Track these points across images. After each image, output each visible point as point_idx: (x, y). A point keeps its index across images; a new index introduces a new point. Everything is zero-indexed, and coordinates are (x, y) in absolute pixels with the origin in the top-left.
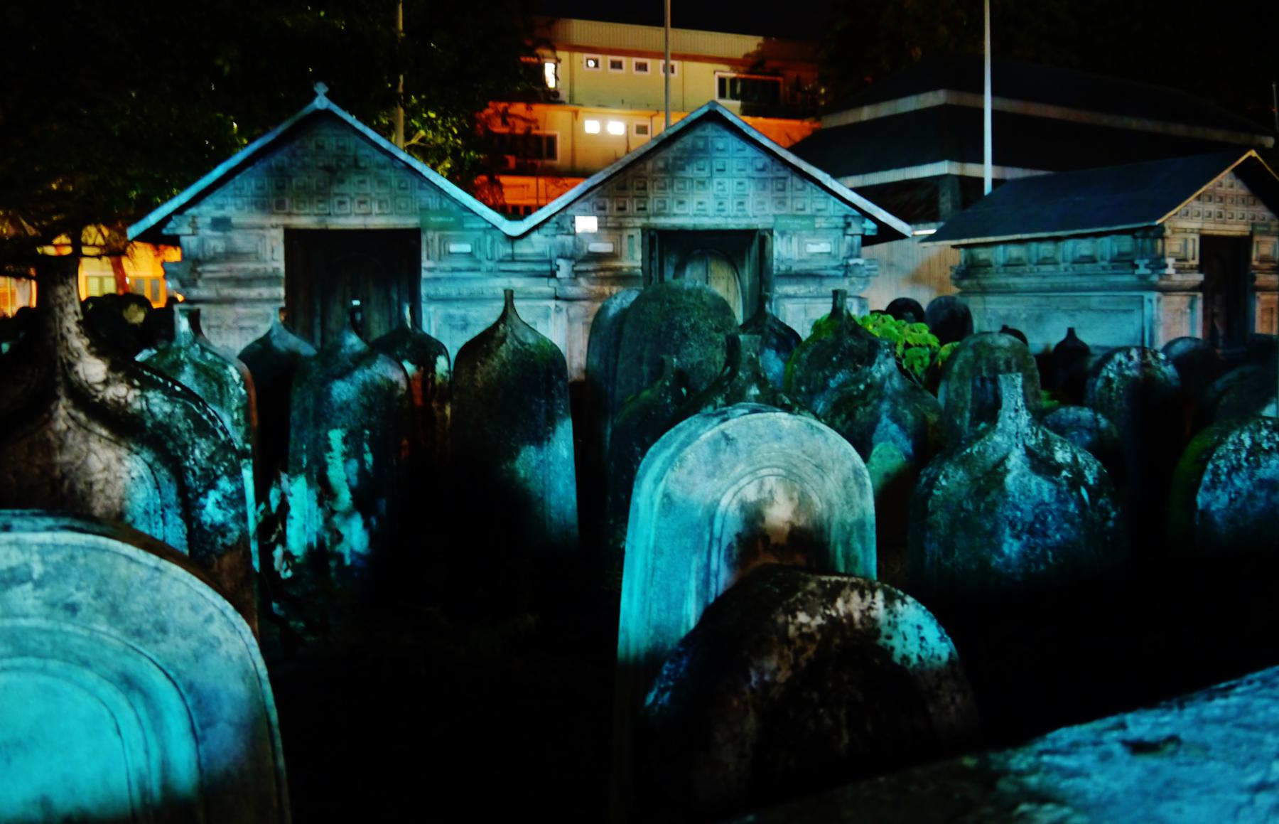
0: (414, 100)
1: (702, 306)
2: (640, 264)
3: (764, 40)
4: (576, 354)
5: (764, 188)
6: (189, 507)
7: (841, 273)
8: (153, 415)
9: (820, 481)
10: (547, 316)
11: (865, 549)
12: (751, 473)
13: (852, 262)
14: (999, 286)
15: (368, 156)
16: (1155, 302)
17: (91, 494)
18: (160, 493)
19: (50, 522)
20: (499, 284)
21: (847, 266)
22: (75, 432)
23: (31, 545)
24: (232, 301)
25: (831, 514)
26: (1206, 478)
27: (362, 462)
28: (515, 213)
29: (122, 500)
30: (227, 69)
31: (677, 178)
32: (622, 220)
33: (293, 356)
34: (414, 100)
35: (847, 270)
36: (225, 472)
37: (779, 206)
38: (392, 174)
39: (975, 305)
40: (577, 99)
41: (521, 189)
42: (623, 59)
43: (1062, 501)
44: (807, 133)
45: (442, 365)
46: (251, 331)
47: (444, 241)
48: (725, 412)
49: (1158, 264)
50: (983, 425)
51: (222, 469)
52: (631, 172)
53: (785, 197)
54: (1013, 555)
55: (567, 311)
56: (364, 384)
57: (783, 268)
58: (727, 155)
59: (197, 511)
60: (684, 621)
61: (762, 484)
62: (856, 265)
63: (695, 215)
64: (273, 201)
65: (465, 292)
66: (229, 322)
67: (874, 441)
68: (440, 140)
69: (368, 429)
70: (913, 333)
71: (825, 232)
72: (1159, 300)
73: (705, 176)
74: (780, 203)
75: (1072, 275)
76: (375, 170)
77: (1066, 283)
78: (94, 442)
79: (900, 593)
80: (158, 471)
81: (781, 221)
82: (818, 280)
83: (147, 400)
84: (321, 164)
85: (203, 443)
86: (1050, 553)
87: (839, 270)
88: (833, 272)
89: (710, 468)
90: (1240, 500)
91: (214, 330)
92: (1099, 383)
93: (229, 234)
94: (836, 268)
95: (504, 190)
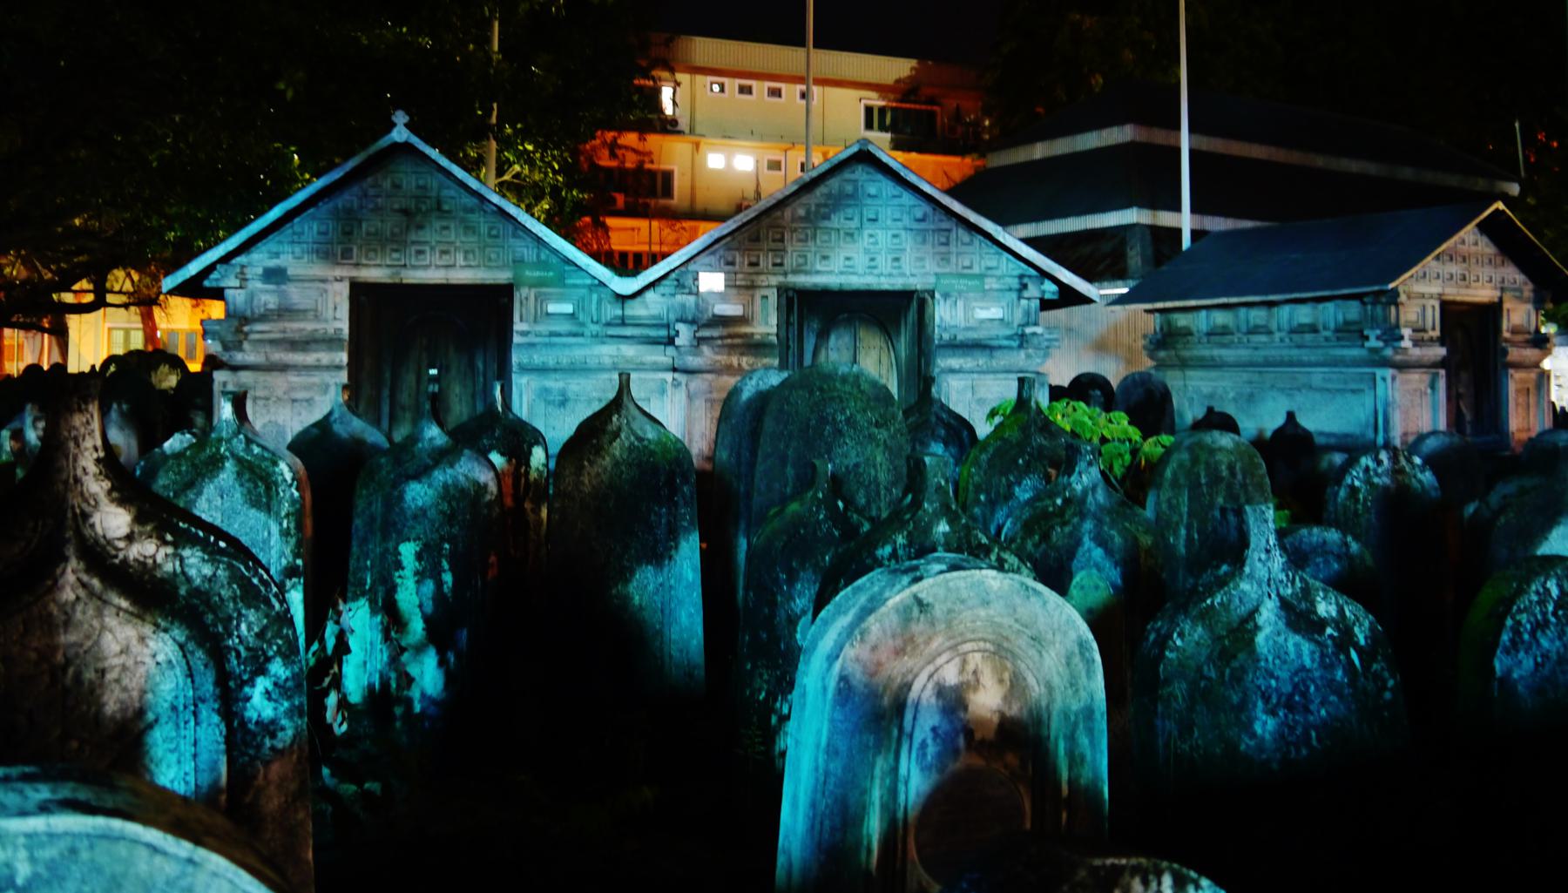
0: (509, 131)
1: (859, 396)
2: (775, 330)
3: (919, 63)
4: (697, 437)
5: (924, 241)
6: (229, 700)
7: (1015, 344)
8: (189, 580)
9: (1037, 657)
10: (663, 392)
11: (1093, 744)
12: (950, 648)
13: (1028, 330)
14: (1202, 358)
15: (452, 198)
16: (1389, 380)
17: (102, 685)
18: (193, 682)
19: (43, 793)
20: (607, 352)
21: (1023, 336)
22: (86, 604)
23: (16, 836)
24: (284, 368)
25: (1051, 701)
26: (1505, 637)
27: (439, 584)
28: (627, 264)
29: (143, 692)
30: (290, 94)
31: (821, 228)
32: (754, 277)
33: (358, 444)
34: (509, 131)
35: (1023, 340)
36: (279, 652)
37: (941, 263)
38: (482, 219)
39: (1174, 381)
40: (698, 130)
41: (630, 232)
42: (754, 83)
43: (1327, 667)
44: (969, 172)
45: (538, 456)
46: (305, 404)
47: (541, 300)
48: (916, 568)
49: (1392, 335)
50: (1225, 568)
51: (275, 648)
52: (766, 221)
53: (949, 253)
54: (1267, 736)
55: (687, 385)
56: (446, 486)
57: (946, 336)
58: (880, 202)
59: (241, 704)
60: (865, 842)
61: (964, 662)
62: (1034, 334)
63: (842, 273)
64: (336, 249)
65: (565, 361)
66: (280, 393)
67: (1074, 569)
68: (537, 177)
69: (448, 543)
70: (1110, 425)
71: (996, 294)
72: (1394, 378)
73: (854, 226)
74: (942, 259)
75: (1290, 347)
76: (461, 214)
77: (1281, 356)
78: (109, 616)
79: (1193, 874)
80: (192, 653)
81: (944, 281)
82: (988, 352)
83: (182, 560)
84: (396, 206)
85: (252, 615)
86: (1313, 734)
87: (1015, 340)
88: (1005, 343)
89: (899, 642)
90: (1548, 666)
91: (261, 403)
92: (1342, 493)
93: (283, 287)
94: (1009, 338)
95: (610, 234)
